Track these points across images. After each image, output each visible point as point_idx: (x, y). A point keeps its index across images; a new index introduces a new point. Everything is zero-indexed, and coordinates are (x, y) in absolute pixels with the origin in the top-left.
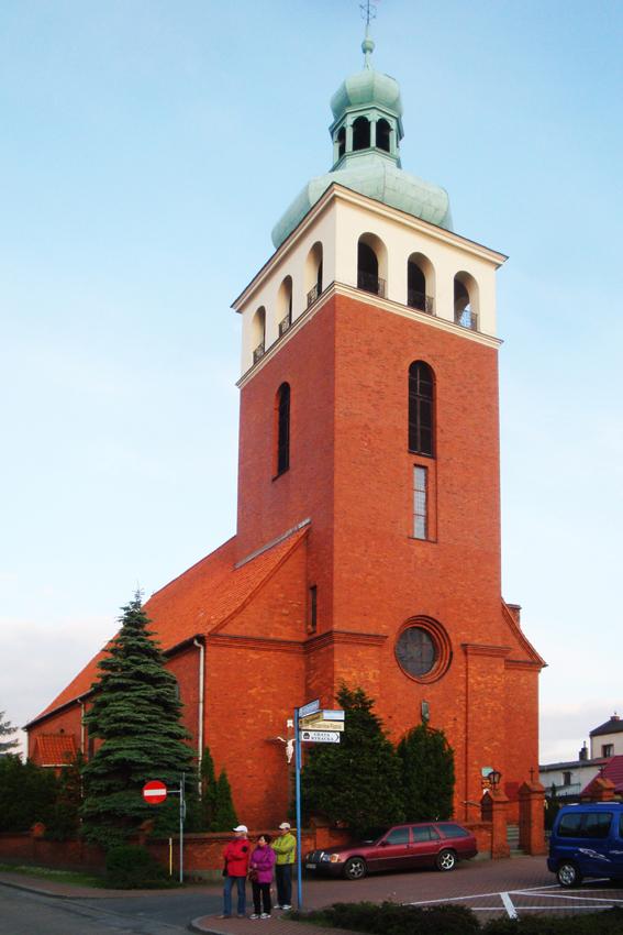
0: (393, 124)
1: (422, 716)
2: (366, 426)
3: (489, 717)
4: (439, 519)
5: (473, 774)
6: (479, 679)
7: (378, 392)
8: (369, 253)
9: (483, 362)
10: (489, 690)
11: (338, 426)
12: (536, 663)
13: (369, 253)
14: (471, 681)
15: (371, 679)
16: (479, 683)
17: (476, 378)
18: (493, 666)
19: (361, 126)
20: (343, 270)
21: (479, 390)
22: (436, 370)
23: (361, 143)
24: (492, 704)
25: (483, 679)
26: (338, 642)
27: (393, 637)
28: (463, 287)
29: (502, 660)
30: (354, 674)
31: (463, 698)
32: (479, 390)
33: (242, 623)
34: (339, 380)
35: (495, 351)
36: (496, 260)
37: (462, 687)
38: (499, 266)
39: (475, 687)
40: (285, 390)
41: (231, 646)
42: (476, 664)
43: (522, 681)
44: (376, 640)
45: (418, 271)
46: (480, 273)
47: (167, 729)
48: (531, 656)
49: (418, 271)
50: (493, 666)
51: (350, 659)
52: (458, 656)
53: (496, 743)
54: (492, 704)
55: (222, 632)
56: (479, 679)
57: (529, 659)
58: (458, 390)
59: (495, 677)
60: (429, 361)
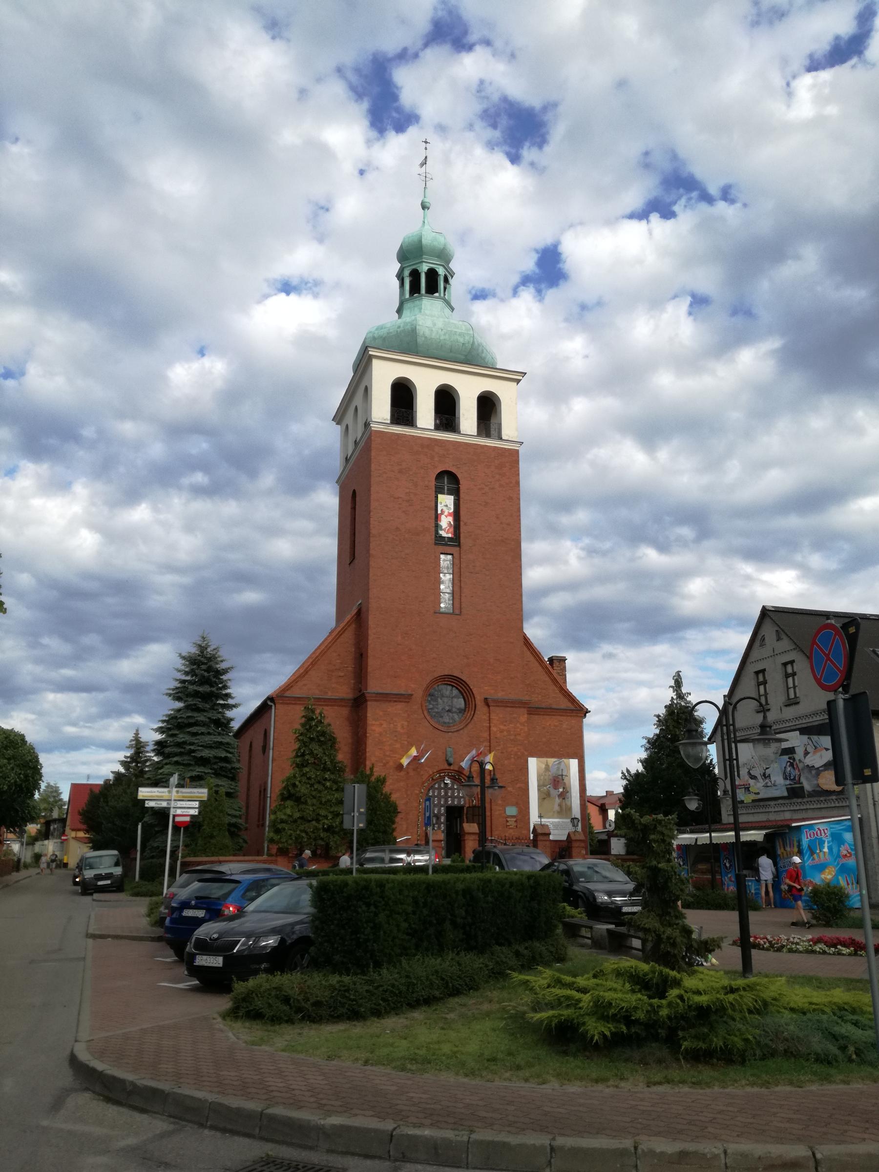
0: (441, 271)
1: (447, 761)
2: (397, 528)
3: (513, 760)
4: (463, 595)
5: (497, 813)
6: (502, 727)
7: (408, 501)
8: (403, 395)
9: (508, 462)
10: (512, 737)
11: (373, 531)
12: (583, 712)
13: (403, 395)
14: (494, 729)
15: (399, 729)
16: (502, 731)
17: (497, 477)
18: (515, 715)
19: (432, 274)
20: (381, 408)
21: (501, 486)
22: (459, 476)
23: (432, 289)
24: (515, 749)
25: (505, 728)
26: (371, 700)
27: (419, 694)
28: (488, 405)
29: (525, 711)
30: (385, 726)
31: (488, 744)
32: (501, 486)
33: (305, 685)
34: (374, 496)
35: (517, 451)
36: (516, 377)
37: (486, 735)
38: (518, 381)
39: (498, 735)
40: (354, 491)
41: (295, 704)
42: (497, 714)
43: (564, 726)
44: (405, 698)
45: (446, 401)
46: (503, 390)
47: (107, 694)
48: (572, 704)
49: (446, 401)
50: (515, 715)
51: (381, 713)
52: (481, 709)
53: (518, 785)
54: (515, 749)
55: (287, 694)
56: (502, 727)
57: (572, 707)
58: (480, 489)
59: (518, 725)
60: (454, 470)
